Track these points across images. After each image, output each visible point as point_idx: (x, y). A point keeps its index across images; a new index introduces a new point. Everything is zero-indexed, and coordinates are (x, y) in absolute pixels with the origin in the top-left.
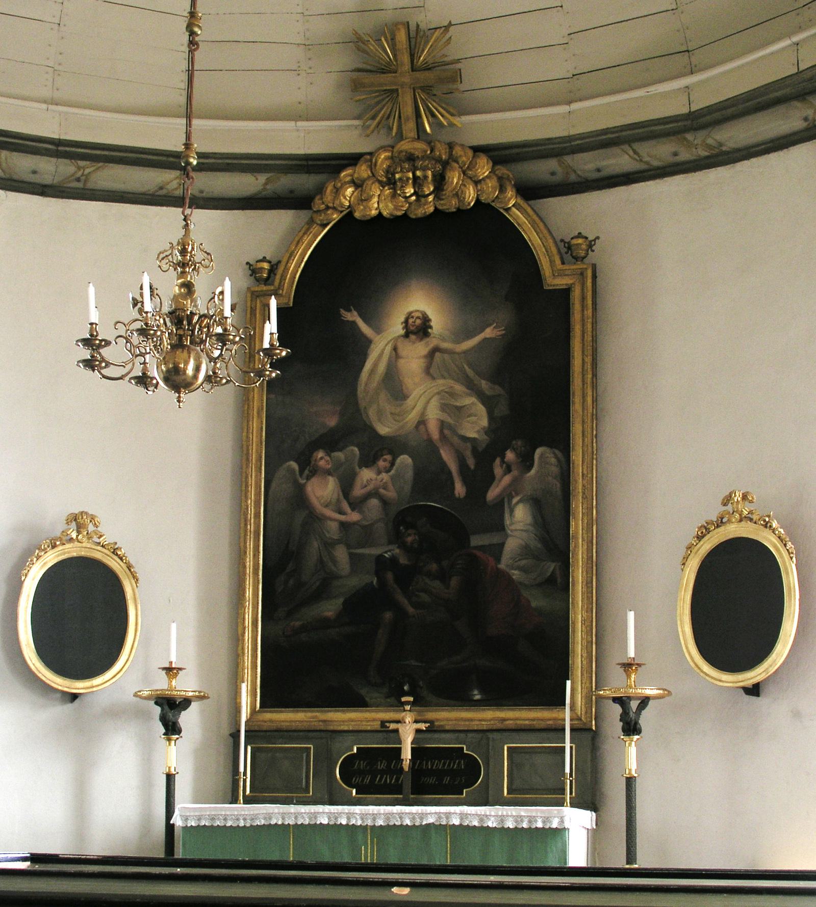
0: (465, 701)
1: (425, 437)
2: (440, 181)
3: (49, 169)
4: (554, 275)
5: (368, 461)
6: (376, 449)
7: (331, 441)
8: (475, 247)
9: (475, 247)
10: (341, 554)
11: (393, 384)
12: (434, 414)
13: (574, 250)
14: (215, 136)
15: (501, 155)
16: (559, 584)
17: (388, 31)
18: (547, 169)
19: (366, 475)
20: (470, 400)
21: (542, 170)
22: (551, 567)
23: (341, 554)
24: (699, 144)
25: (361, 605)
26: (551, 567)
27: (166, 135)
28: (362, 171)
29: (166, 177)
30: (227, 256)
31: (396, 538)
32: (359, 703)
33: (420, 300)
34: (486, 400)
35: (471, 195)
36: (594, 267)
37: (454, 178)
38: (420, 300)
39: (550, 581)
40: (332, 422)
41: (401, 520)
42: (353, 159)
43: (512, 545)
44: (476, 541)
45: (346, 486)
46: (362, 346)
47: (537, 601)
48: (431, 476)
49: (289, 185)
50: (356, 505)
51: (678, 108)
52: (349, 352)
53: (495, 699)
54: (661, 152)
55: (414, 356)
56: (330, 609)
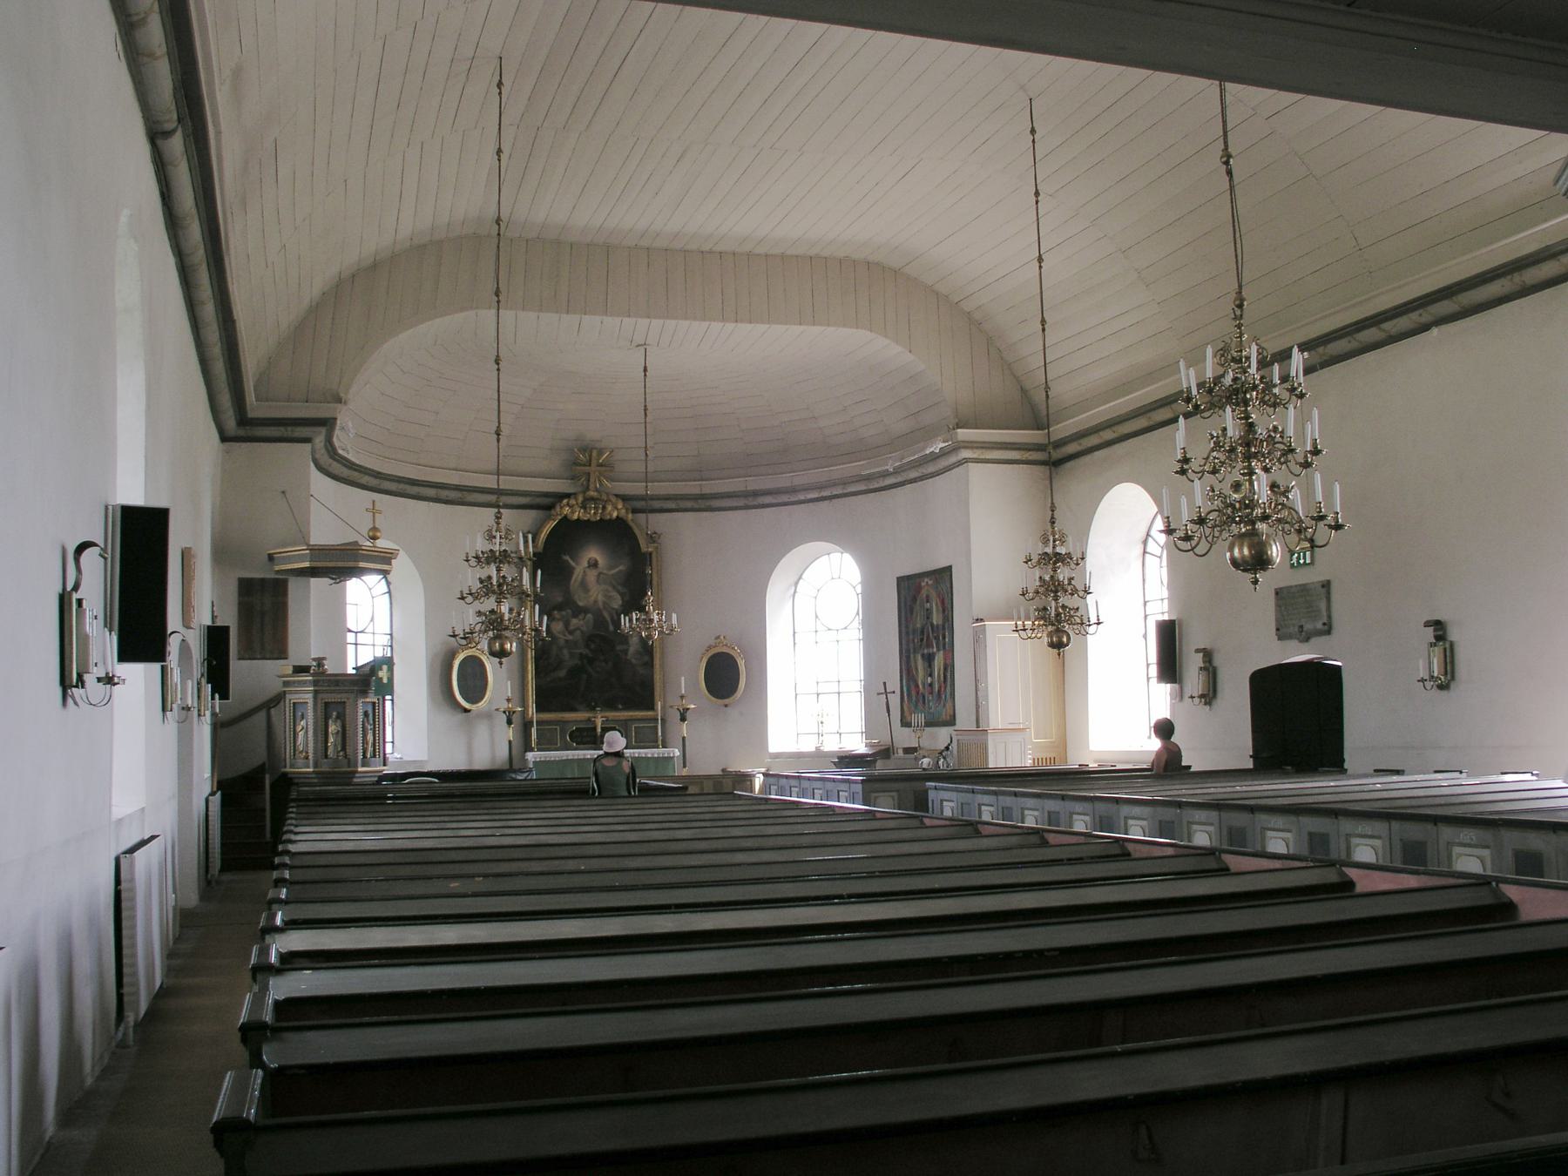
0: (616, 709)
1: (259, 756)
2: (604, 508)
3: (453, 495)
4: (645, 547)
5: (575, 616)
6: (579, 611)
7: (560, 607)
8: (617, 534)
9: (617, 534)
10: (565, 652)
11: (584, 585)
12: (600, 598)
13: (653, 538)
14: (507, 483)
15: (625, 498)
16: (650, 665)
17: (584, 450)
18: (643, 505)
19: (574, 621)
20: (614, 594)
21: (640, 504)
22: (646, 658)
23: (565, 652)
24: (702, 504)
25: (574, 672)
26: (646, 658)
27: (490, 482)
28: (573, 502)
29: (496, 499)
30: (521, 532)
31: (587, 646)
32: (573, 710)
33: (593, 553)
34: (622, 595)
35: (615, 514)
36: (1452, 644)
37: (609, 508)
38: (593, 553)
39: (646, 664)
40: (560, 599)
41: (589, 639)
42: (568, 496)
43: (632, 650)
44: (619, 648)
45: (567, 624)
46: (570, 571)
47: (641, 671)
48: (599, 622)
49: (546, 503)
50: (571, 633)
51: (697, 491)
52: (567, 572)
53: (627, 708)
54: (689, 504)
55: (592, 576)
56: (562, 673)
